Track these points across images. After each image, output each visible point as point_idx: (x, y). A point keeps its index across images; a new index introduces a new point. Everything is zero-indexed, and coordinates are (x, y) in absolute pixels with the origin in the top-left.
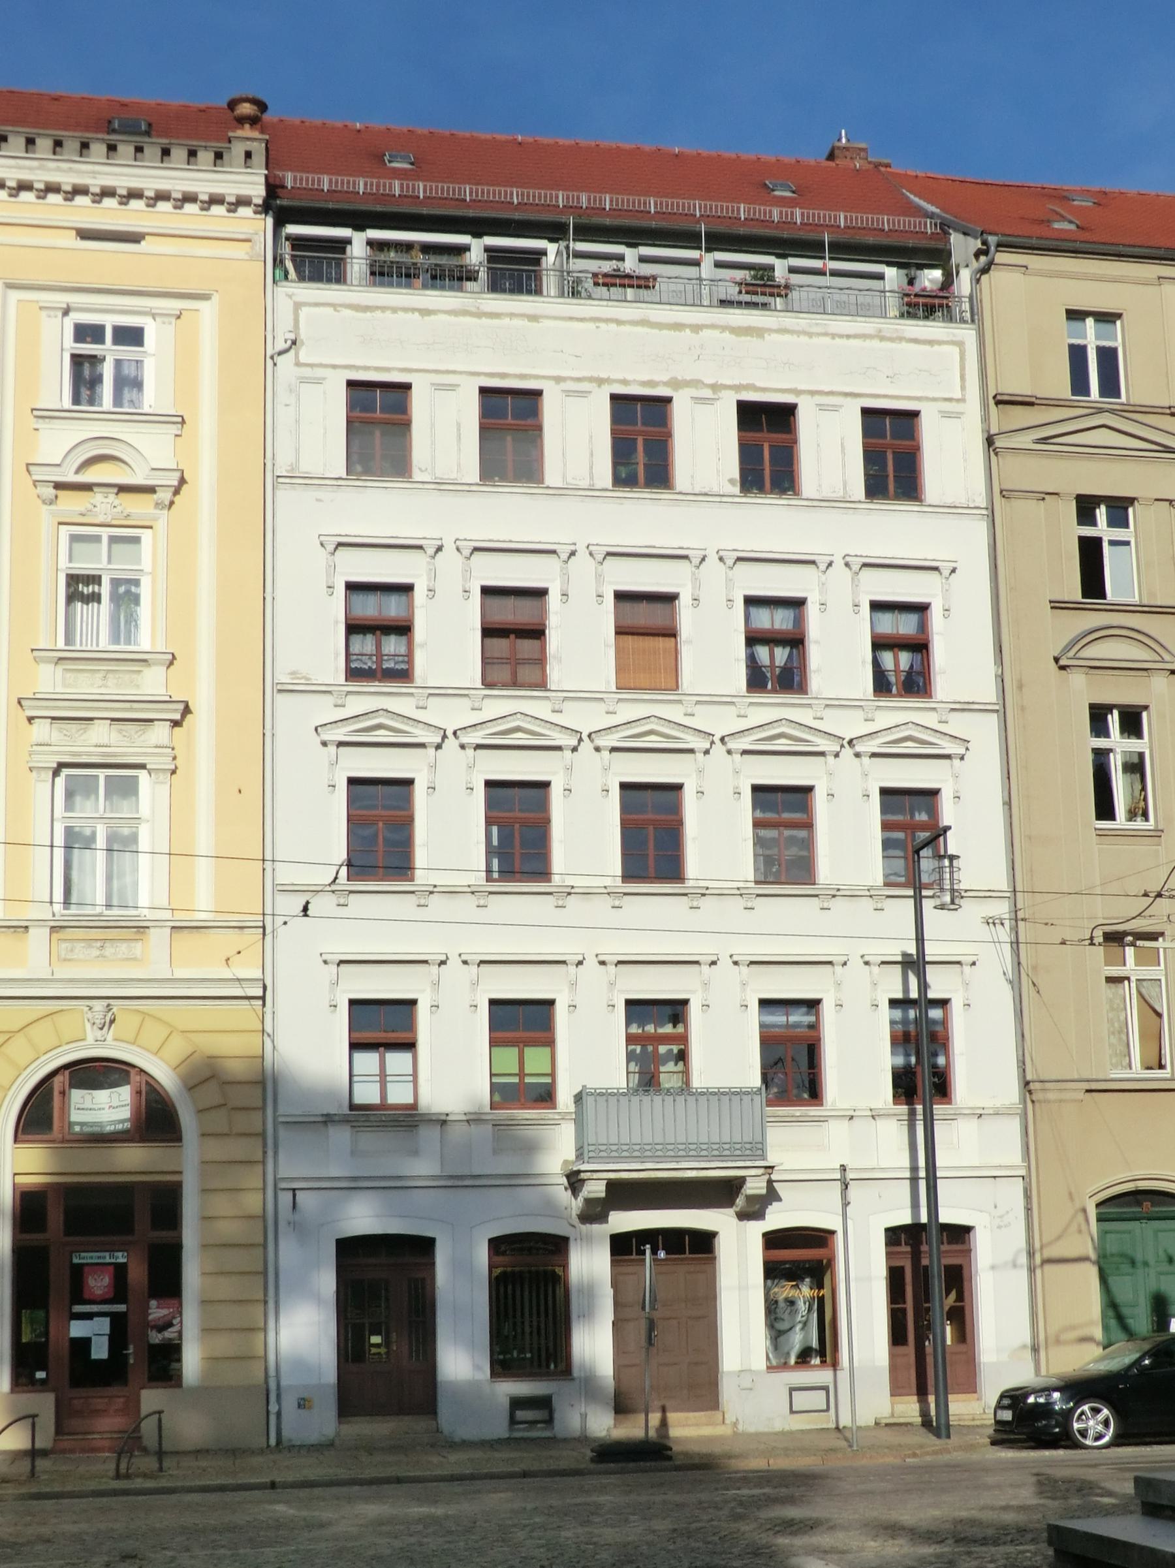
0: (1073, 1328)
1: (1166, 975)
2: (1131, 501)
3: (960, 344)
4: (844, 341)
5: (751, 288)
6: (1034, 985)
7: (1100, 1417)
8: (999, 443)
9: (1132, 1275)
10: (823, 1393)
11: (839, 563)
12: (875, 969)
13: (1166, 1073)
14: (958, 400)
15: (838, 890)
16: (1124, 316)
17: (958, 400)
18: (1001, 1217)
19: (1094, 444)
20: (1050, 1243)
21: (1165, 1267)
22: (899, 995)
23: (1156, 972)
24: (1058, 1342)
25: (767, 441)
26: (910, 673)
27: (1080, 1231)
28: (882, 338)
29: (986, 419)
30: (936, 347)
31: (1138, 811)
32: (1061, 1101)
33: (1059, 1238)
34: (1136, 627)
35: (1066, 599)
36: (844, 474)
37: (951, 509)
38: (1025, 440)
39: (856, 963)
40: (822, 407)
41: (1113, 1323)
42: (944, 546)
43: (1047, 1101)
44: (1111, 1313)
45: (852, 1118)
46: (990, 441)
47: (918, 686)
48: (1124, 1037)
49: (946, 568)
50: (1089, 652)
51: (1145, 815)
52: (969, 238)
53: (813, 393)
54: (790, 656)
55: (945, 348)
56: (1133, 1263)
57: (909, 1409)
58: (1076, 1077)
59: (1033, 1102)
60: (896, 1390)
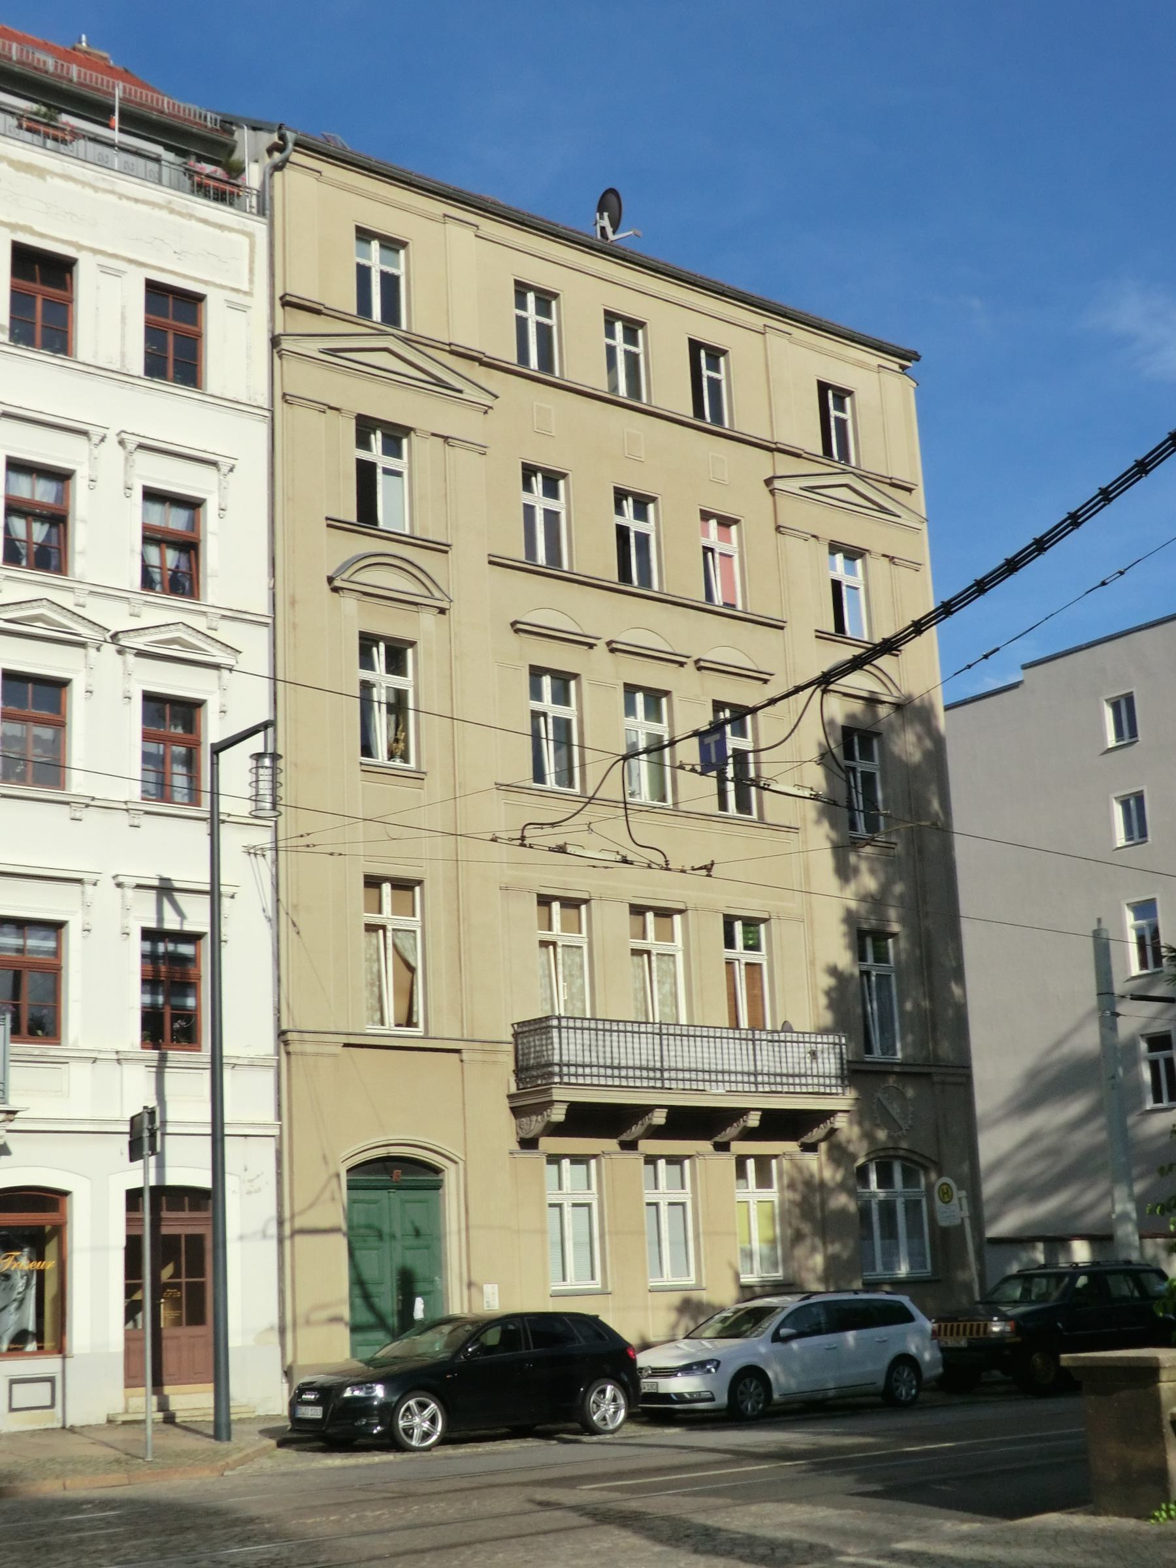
0: (323, 1307)
1: (423, 928)
2: (407, 431)
3: (250, 235)
4: (132, 204)
5: (32, 125)
6: (294, 925)
7: (426, 1413)
8: (286, 344)
9: (377, 1249)
10: (48, 1385)
11: (112, 439)
12: (130, 893)
13: (419, 1031)
14: (245, 293)
15: (93, 799)
16: (411, 246)
17: (245, 293)
18: (251, 1181)
19: (377, 365)
20: (302, 1213)
21: (411, 1241)
22: (152, 924)
23: (414, 923)
24: (308, 1322)
25: (41, 291)
26: (175, 572)
27: (333, 1199)
28: (172, 211)
29: (272, 319)
30: (226, 233)
31: (398, 750)
32: (317, 1054)
33: (311, 1206)
34: (411, 559)
35: (342, 518)
36: (123, 345)
37: (234, 404)
38: (311, 347)
39: (107, 883)
40: (104, 270)
41: (359, 1301)
42: (225, 437)
43: (302, 1054)
44: (357, 1291)
45: (95, 1060)
46: (275, 341)
47: (184, 588)
48: (376, 990)
49: (225, 464)
50: (363, 577)
51: (405, 758)
52: (260, 133)
53: (95, 251)
54: (48, 535)
55: (234, 236)
56: (380, 1236)
57: (143, 1403)
58: (333, 1030)
59: (288, 1053)
60: (131, 1380)
